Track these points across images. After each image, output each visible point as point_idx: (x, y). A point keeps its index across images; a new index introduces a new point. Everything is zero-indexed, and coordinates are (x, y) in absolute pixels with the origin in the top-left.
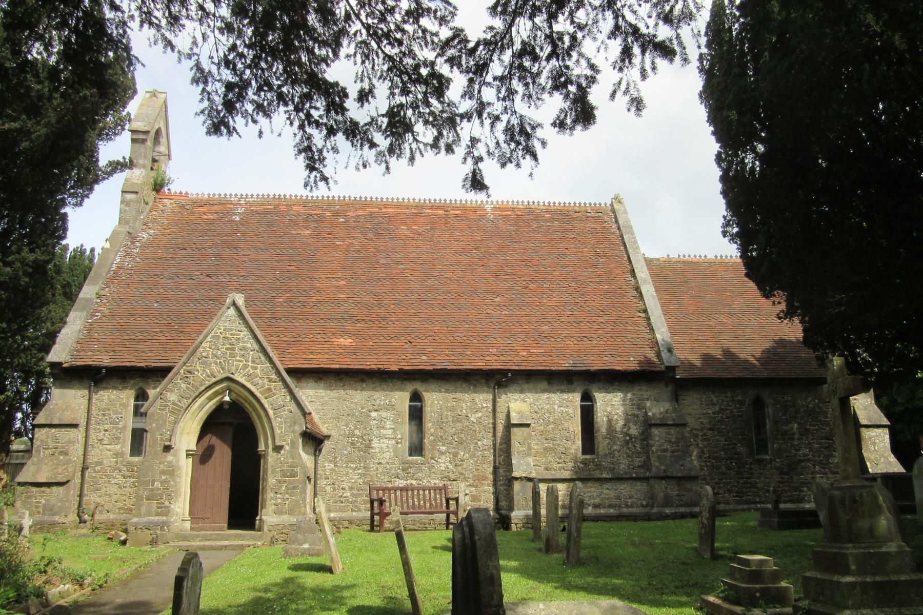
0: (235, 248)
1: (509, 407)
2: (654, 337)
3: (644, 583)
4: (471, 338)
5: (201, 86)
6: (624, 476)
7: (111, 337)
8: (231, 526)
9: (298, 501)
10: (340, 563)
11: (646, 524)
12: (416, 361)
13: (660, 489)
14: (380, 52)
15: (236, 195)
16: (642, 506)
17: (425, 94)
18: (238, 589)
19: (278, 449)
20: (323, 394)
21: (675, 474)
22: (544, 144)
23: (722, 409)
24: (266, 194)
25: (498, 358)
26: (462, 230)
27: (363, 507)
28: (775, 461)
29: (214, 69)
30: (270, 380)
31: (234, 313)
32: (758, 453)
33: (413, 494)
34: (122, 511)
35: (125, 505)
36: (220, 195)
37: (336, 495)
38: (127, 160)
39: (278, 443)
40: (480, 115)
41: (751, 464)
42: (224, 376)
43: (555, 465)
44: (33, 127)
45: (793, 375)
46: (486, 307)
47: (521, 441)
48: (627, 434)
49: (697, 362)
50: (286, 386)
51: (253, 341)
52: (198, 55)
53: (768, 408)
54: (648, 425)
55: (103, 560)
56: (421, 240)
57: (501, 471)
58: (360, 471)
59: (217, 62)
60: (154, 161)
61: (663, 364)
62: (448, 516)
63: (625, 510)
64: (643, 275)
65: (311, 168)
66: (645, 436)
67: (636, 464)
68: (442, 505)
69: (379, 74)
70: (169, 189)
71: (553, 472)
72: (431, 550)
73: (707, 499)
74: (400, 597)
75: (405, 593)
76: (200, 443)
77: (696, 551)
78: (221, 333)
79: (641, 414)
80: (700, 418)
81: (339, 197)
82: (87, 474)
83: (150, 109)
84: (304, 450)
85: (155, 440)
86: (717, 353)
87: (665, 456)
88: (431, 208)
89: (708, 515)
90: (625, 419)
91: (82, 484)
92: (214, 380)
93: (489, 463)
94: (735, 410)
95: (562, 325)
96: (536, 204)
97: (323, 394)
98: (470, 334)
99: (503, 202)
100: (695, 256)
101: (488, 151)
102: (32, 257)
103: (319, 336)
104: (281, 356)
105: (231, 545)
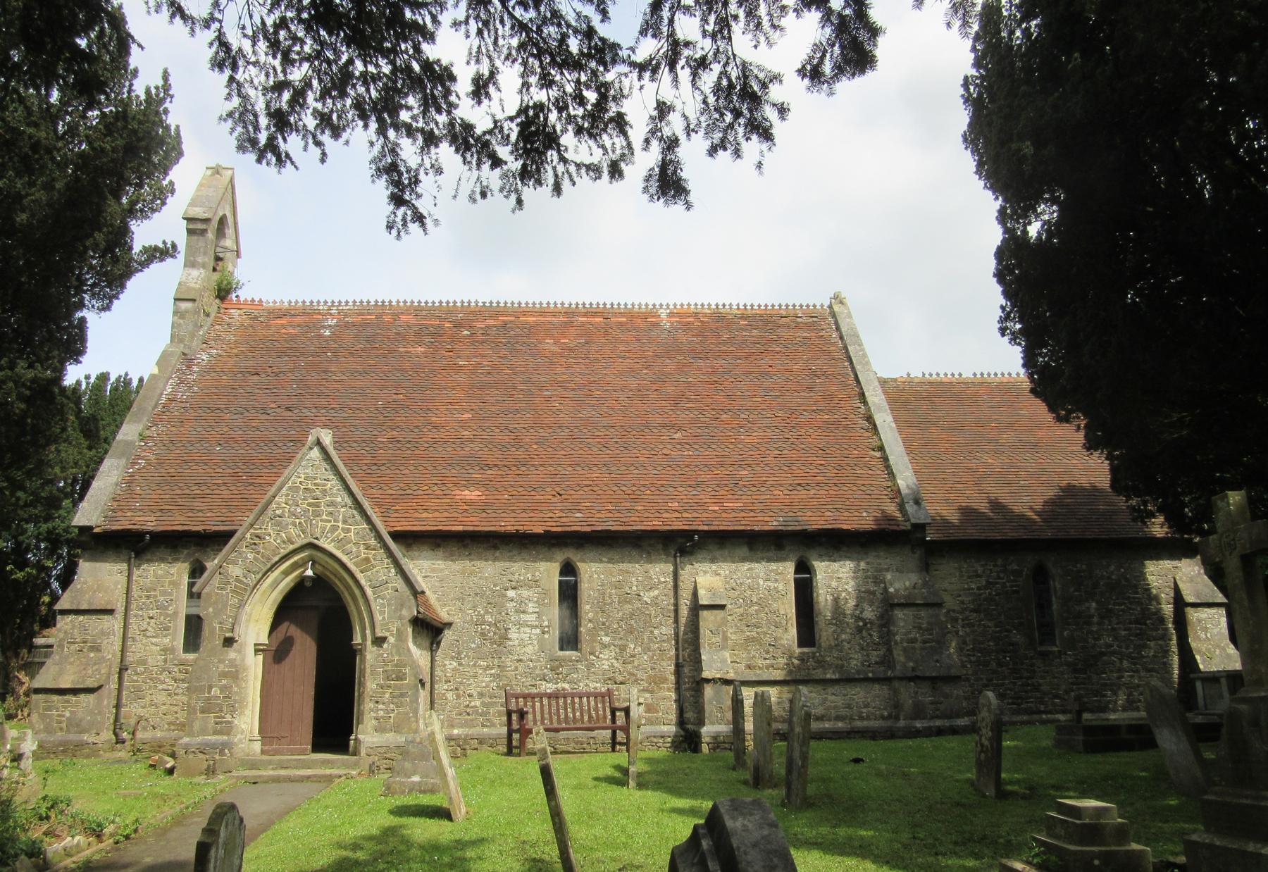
0: (324, 372)
1: (695, 582)
2: (895, 484)
3: (905, 836)
4: (642, 489)
5: (228, 72)
6: (857, 676)
7: (160, 492)
8: (317, 748)
9: (407, 713)
10: (463, 806)
11: (890, 744)
12: (568, 519)
13: (907, 695)
14: (506, 17)
15: (326, 302)
16: (883, 718)
17: (578, 82)
18: (316, 846)
19: (379, 641)
20: (443, 566)
21: (928, 674)
22: (782, 110)
23: (991, 583)
24: (365, 300)
25: (679, 515)
26: (627, 344)
27: (497, 720)
28: (1065, 654)
29: (247, 45)
30: (368, 547)
31: (318, 455)
32: (1041, 644)
33: (565, 703)
34: (172, 727)
35: (177, 718)
36: (304, 302)
37: (460, 704)
38: (169, 246)
39: (379, 634)
40: (672, 65)
41: (1032, 658)
42: (305, 541)
43: (760, 662)
44: (24, 188)
45: (1089, 535)
46: (661, 446)
47: (713, 629)
48: (859, 618)
49: (954, 518)
50: (390, 554)
51: (345, 494)
52: (220, 21)
53: (1054, 581)
54: (889, 605)
55: (137, 797)
56: (572, 358)
57: (686, 670)
58: (493, 671)
59: (250, 33)
60: (218, 259)
61: (909, 520)
62: (614, 733)
63: (859, 724)
64: (876, 400)
65: (398, 200)
66: (885, 621)
67: (874, 659)
68: (605, 717)
69: (505, 51)
70: (237, 296)
71: (758, 672)
72: (591, 783)
73: (989, 711)
74: (547, 858)
75: (555, 853)
76: (274, 634)
77: (972, 784)
78: (301, 483)
79: (878, 590)
80: (960, 596)
81: (463, 302)
82: (126, 677)
83: (212, 189)
84: (415, 643)
85: (213, 631)
86: (983, 506)
87: (914, 648)
88: (586, 314)
89: (990, 733)
90: (857, 598)
91: (120, 690)
92: (291, 547)
93: (670, 659)
94: (1008, 584)
95: (767, 468)
96: (727, 307)
97: (443, 566)
98: (642, 482)
99: (682, 305)
100: (946, 374)
101: (688, 125)
102: (31, 374)
103: (436, 488)
104: (385, 514)
105: (315, 776)
